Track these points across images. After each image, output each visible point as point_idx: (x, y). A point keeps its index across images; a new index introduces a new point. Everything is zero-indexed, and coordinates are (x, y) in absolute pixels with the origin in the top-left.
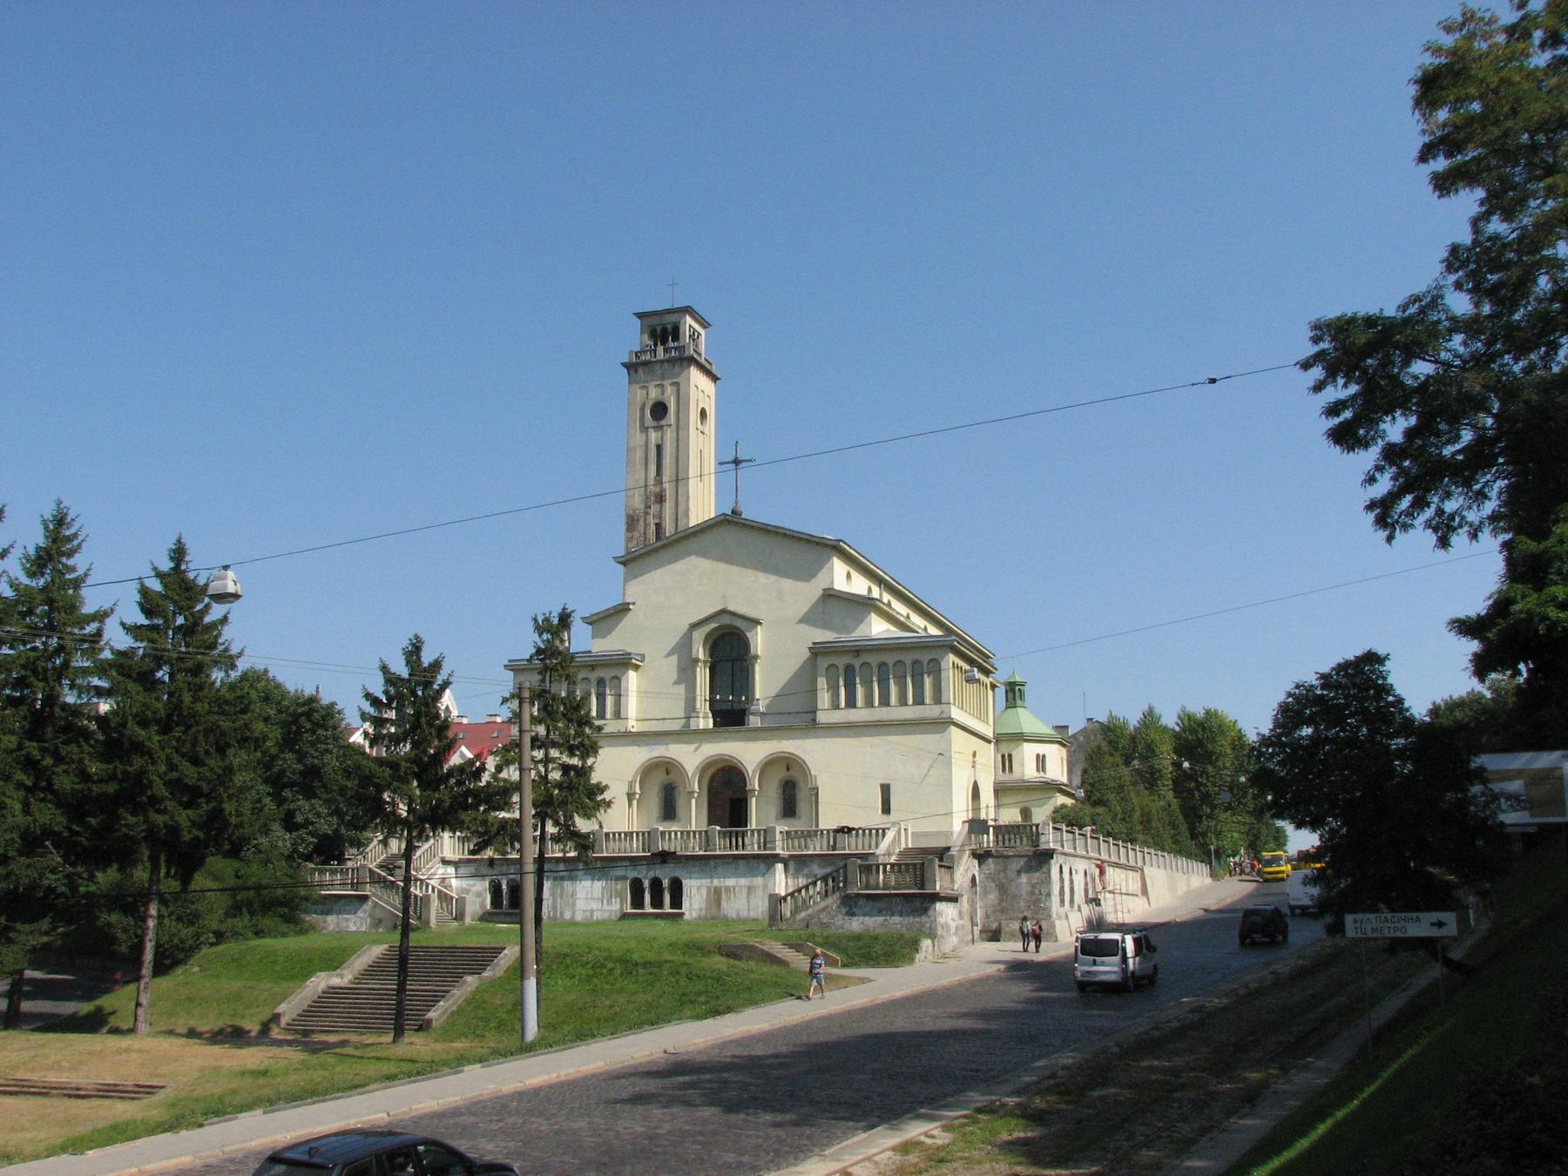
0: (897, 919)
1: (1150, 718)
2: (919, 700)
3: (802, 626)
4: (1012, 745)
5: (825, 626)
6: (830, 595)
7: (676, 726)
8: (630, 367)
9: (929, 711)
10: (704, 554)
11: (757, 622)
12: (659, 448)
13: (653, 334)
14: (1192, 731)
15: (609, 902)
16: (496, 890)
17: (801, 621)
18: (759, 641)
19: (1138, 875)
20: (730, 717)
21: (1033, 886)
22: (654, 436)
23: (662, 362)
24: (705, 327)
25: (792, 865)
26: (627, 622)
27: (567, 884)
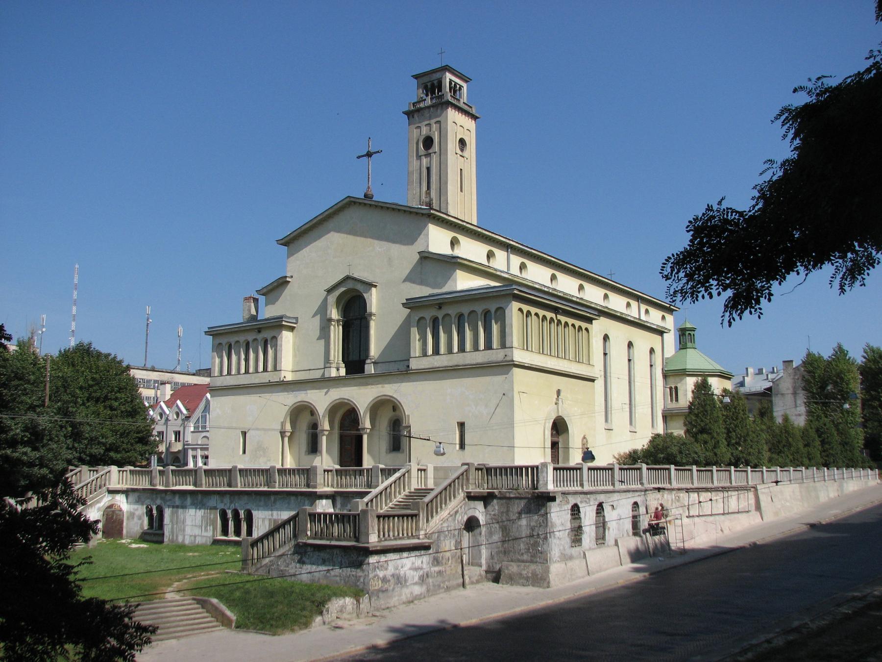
0: (337, 571)
1: (840, 353)
2: (489, 346)
3: (408, 284)
4: (677, 379)
5: (422, 283)
6: (426, 257)
7: (317, 375)
8: (409, 114)
9: (496, 355)
10: (339, 231)
11: (370, 285)
12: (428, 169)
13: (426, 88)
14: (875, 361)
15: (206, 530)
16: (149, 513)
17: (405, 281)
18: (374, 300)
19: (751, 495)
20: (355, 363)
21: (533, 529)
22: (425, 161)
23: (429, 107)
24: (466, 82)
25: (339, 500)
26: (288, 291)
27: (180, 511)
